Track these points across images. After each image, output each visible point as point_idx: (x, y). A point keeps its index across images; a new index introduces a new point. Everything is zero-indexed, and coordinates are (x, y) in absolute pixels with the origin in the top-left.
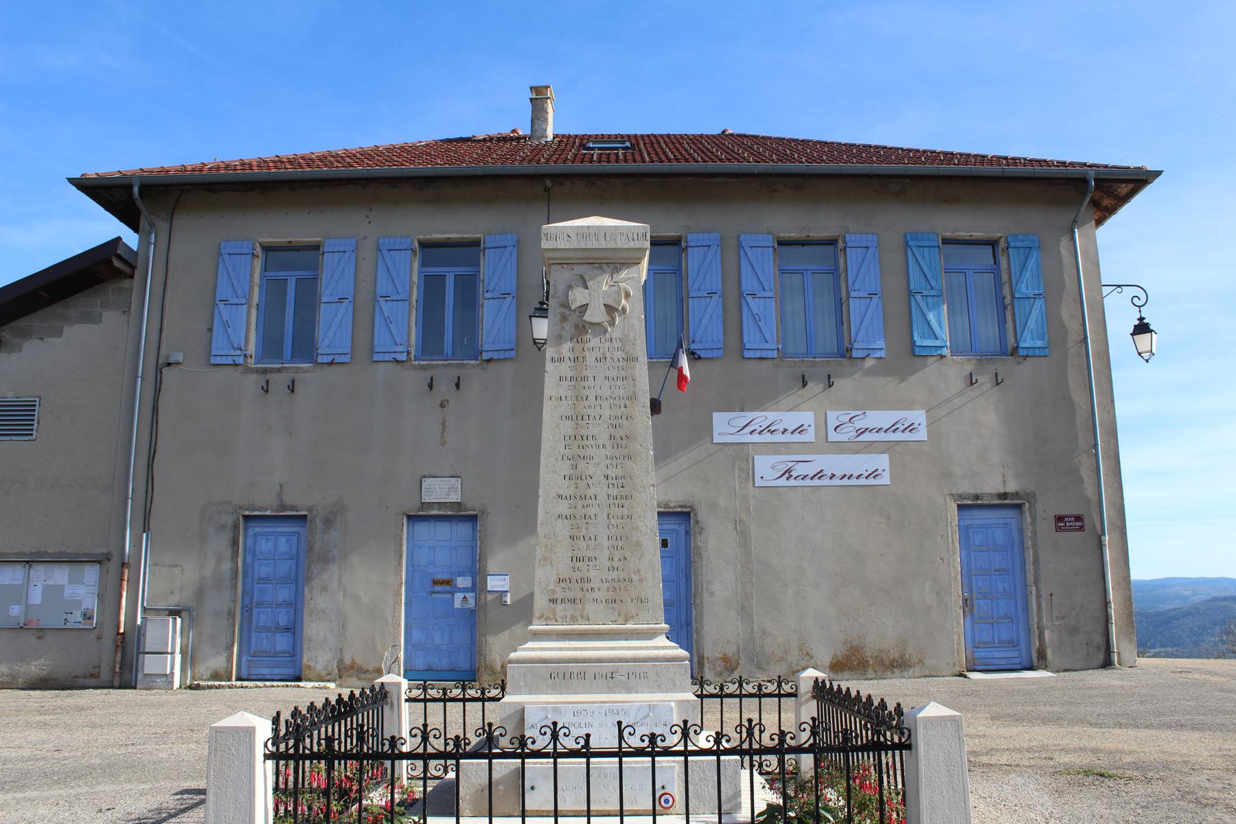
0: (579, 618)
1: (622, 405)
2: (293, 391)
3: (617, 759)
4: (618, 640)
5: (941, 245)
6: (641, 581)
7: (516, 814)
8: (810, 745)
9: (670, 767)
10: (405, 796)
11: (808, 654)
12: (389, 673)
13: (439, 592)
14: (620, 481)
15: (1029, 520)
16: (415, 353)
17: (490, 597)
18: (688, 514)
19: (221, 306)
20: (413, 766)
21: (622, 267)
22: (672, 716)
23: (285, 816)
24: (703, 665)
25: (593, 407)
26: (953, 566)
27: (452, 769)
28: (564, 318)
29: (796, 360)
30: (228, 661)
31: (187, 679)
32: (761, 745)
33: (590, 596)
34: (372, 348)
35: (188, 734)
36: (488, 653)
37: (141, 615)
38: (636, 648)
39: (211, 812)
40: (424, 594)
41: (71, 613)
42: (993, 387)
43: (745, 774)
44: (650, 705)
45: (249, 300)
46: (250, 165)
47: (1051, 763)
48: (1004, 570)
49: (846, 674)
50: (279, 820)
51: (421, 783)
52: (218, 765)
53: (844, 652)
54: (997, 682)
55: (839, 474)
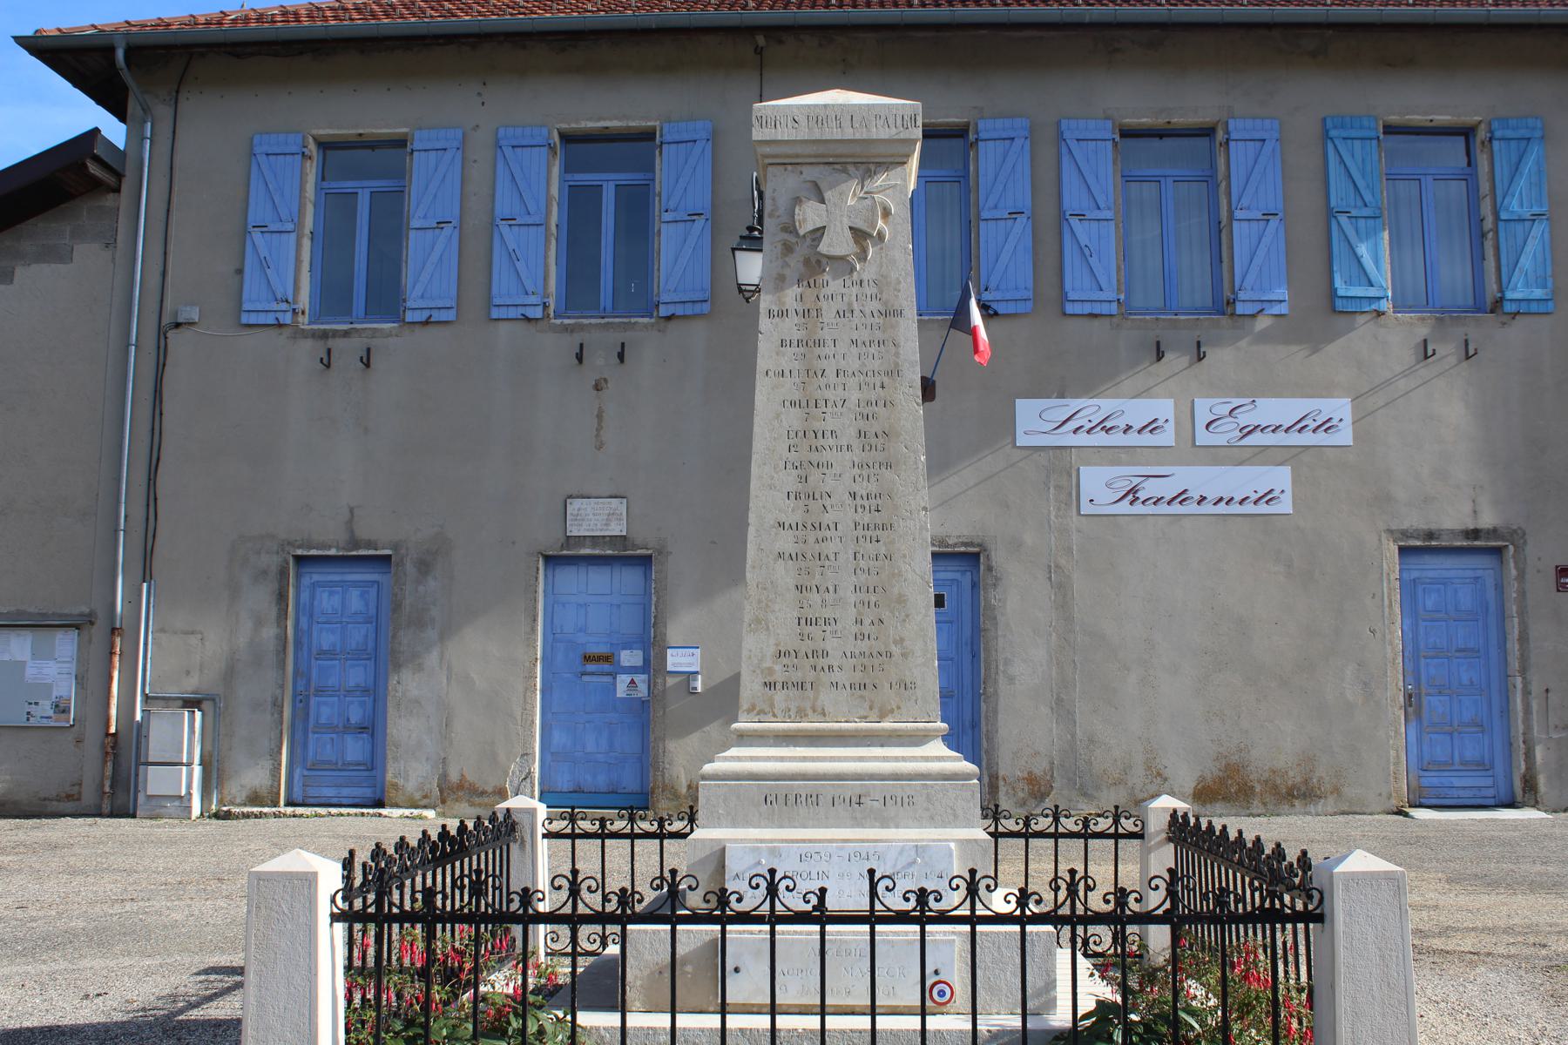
0: (810, 712)
2: (368, 365)
3: (866, 928)
4: (869, 746)
5: (1382, 136)
6: (904, 655)
7: (711, 1009)
8: (1166, 912)
9: (948, 940)
10: (543, 981)
11: (1159, 774)
12: (517, 795)
13: (592, 674)
14: (873, 502)
15: (1514, 572)
16: (556, 307)
17: (671, 681)
18: (976, 556)
19: (256, 235)
20: (555, 936)
22: (951, 863)
23: (363, 1007)
24: (997, 787)
26: (1391, 643)
27: (614, 940)
28: (788, 249)
29: (1147, 317)
30: (273, 776)
31: (210, 805)
32: (1086, 909)
33: (826, 678)
34: (490, 298)
35: (214, 884)
36: (667, 766)
37: (141, 707)
38: (896, 759)
39: (252, 1000)
40: (569, 675)
41: (36, 704)
42: (1460, 362)
43: (1063, 956)
44: (917, 846)
45: (299, 226)
46: (296, 14)
47: (1544, 952)
48: (1472, 650)
49: (1219, 807)
50: (354, 1013)
51: (568, 961)
52: (261, 928)
53: (1216, 773)
54: (1457, 825)
55: (1212, 496)
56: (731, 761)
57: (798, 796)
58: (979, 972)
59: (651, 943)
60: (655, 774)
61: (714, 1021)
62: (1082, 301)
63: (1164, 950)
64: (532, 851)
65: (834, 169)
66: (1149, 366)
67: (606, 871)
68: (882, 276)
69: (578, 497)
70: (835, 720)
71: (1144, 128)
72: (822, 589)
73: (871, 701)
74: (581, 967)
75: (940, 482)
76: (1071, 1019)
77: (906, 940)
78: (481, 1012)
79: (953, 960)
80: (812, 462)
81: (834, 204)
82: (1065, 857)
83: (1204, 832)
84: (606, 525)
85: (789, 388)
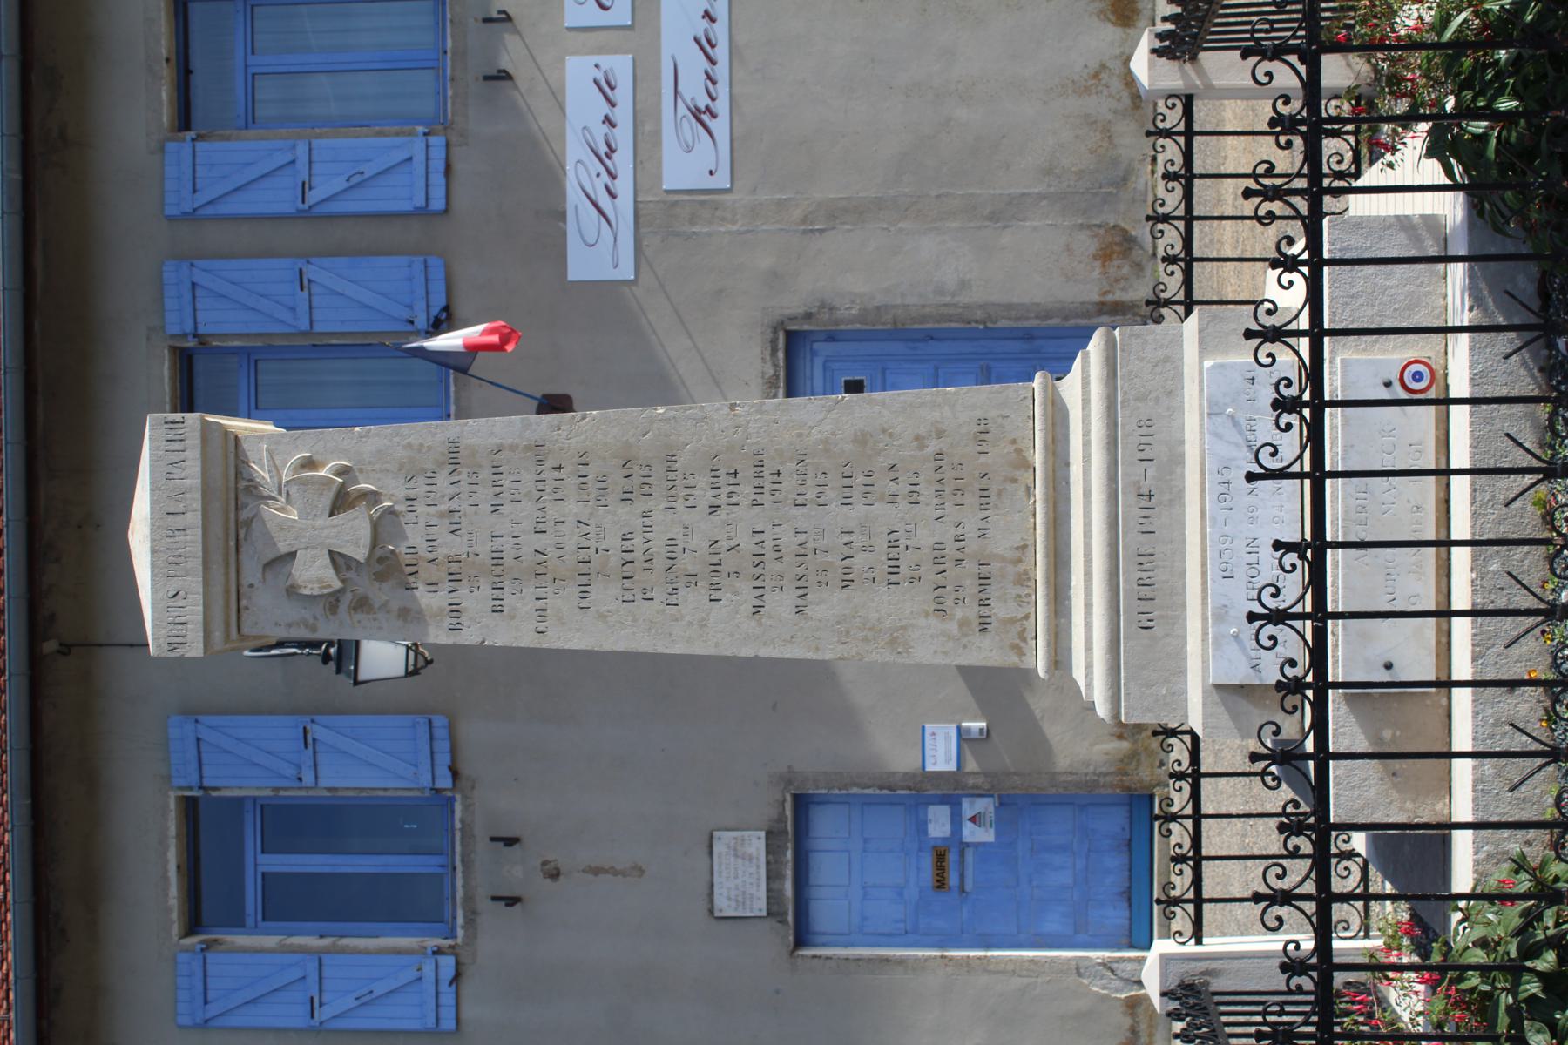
0: (1021, 567)
1: (556, 474)
4: (1068, 483)
6: (940, 434)
7: (1444, 701)
11: (1096, 75)
13: (962, 877)
14: (723, 480)
18: (790, 335)
27: (1344, 841)
28: (362, 604)
29: (450, 93)
32: (1299, 175)
33: (972, 545)
36: (1091, 768)
38: (1086, 444)
43: (1359, 206)
44: (1209, 414)
51: (1375, 906)
57: (1141, 582)
58: (1387, 324)
59: (1354, 787)
60: (1103, 786)
61: (1462, 699)
62: (427, 186)
63: (1349, 65)
64: (1221, 959)
65: (245, 539)
66: (519, 91)
67: (1243, 853)
68: (400, 470)
69: (711, 901)
70: (1032, 531)
71: (175, 94)
72: (847, 551)
73: (1005, 481)
74: (1384, 888)
75: (685, 386)
76: (1452, 193)
77: (1343, 429)
78: (1458, 1030)
79: (1372, 362)
80: (668, 567)
82: (1215, 206)
83: (1184, 10)
84: (751, 859)
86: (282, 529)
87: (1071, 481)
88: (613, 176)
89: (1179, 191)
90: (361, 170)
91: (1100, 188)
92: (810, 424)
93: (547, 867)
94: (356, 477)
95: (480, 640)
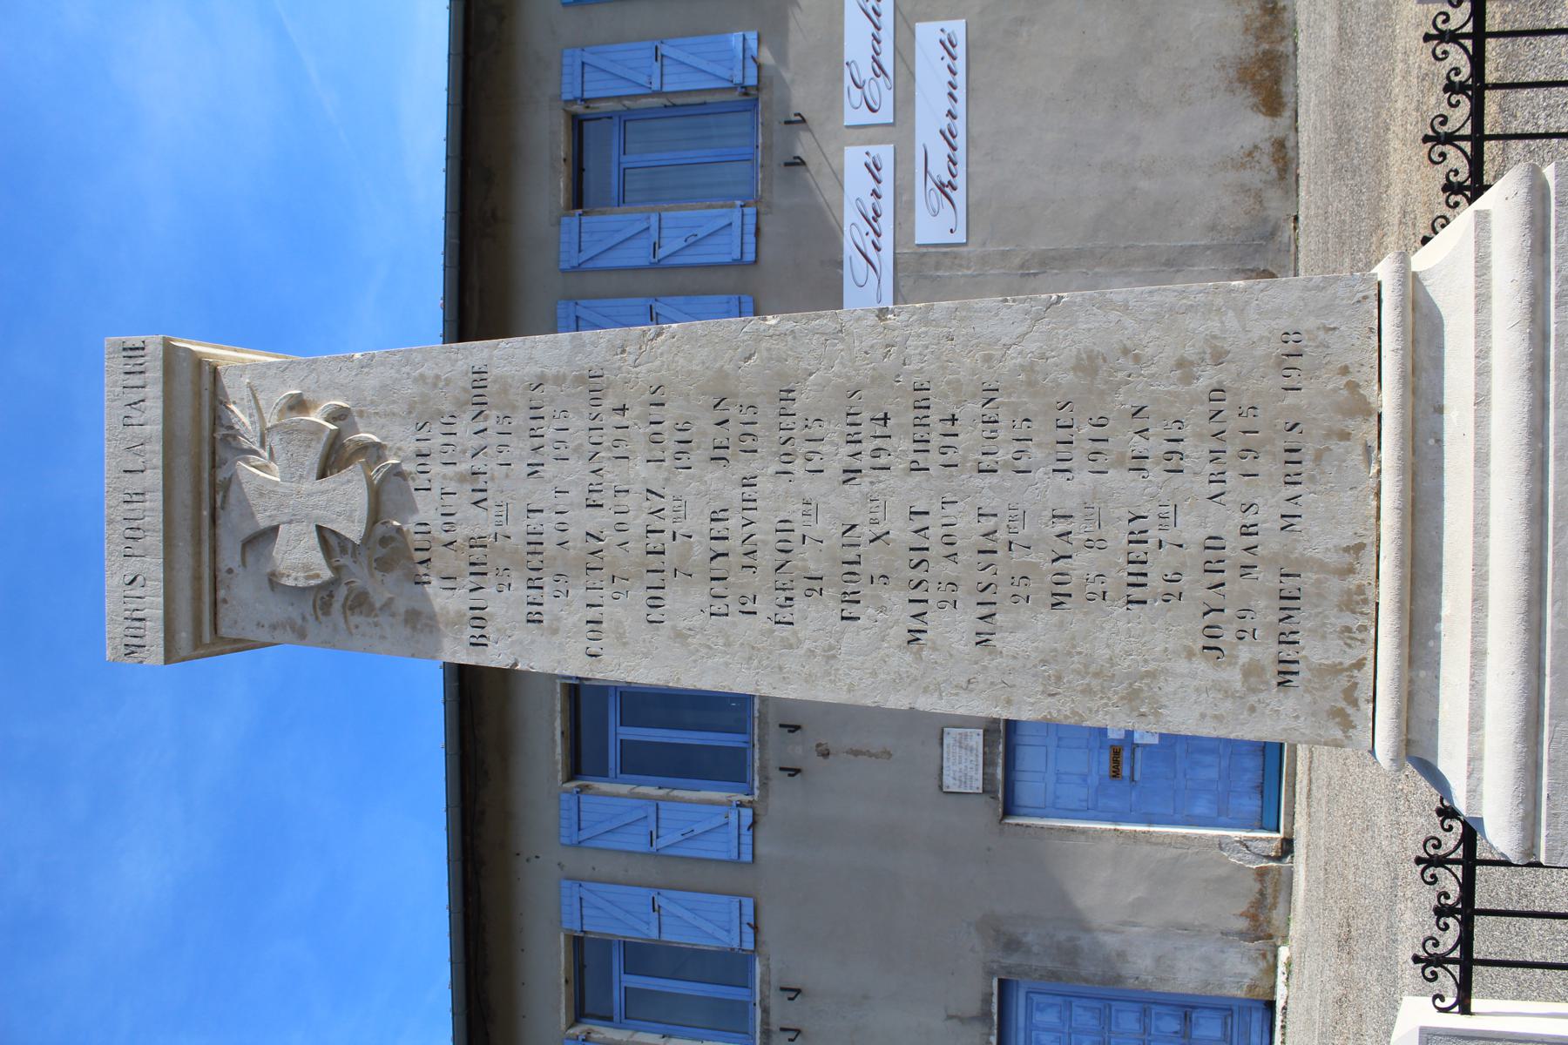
0: (1353, 582)
1: (617, 419)
2: (798, 991)
4: (1439, 441)
6: (1219, 358)
11: (1250, 154)
14: (866, 429)
16: (742, 793)
21: (224, 422)
25: (621, 518)
29: (760, 176)
33: (1270, 542)
38: (1483, 372)
40: (1133, 794)
55: (947, 104)
56: (1480, 780)
62: (742, 244)
65: (223, 508)
68: (410, 412)
70: (1373, 520)
71: (571, 185)
72: (1061, 547)
81: (277, 509)
85: (625, 610)
86: (261, 495)
87: (1446, 438)
88: (878, 235)
89: (1465, 106)
90: (695, 233)
91: (1253, 240)
92: (1005, 340)
93: (820, 748)
94: (355, 424)
95: (511, 662)
